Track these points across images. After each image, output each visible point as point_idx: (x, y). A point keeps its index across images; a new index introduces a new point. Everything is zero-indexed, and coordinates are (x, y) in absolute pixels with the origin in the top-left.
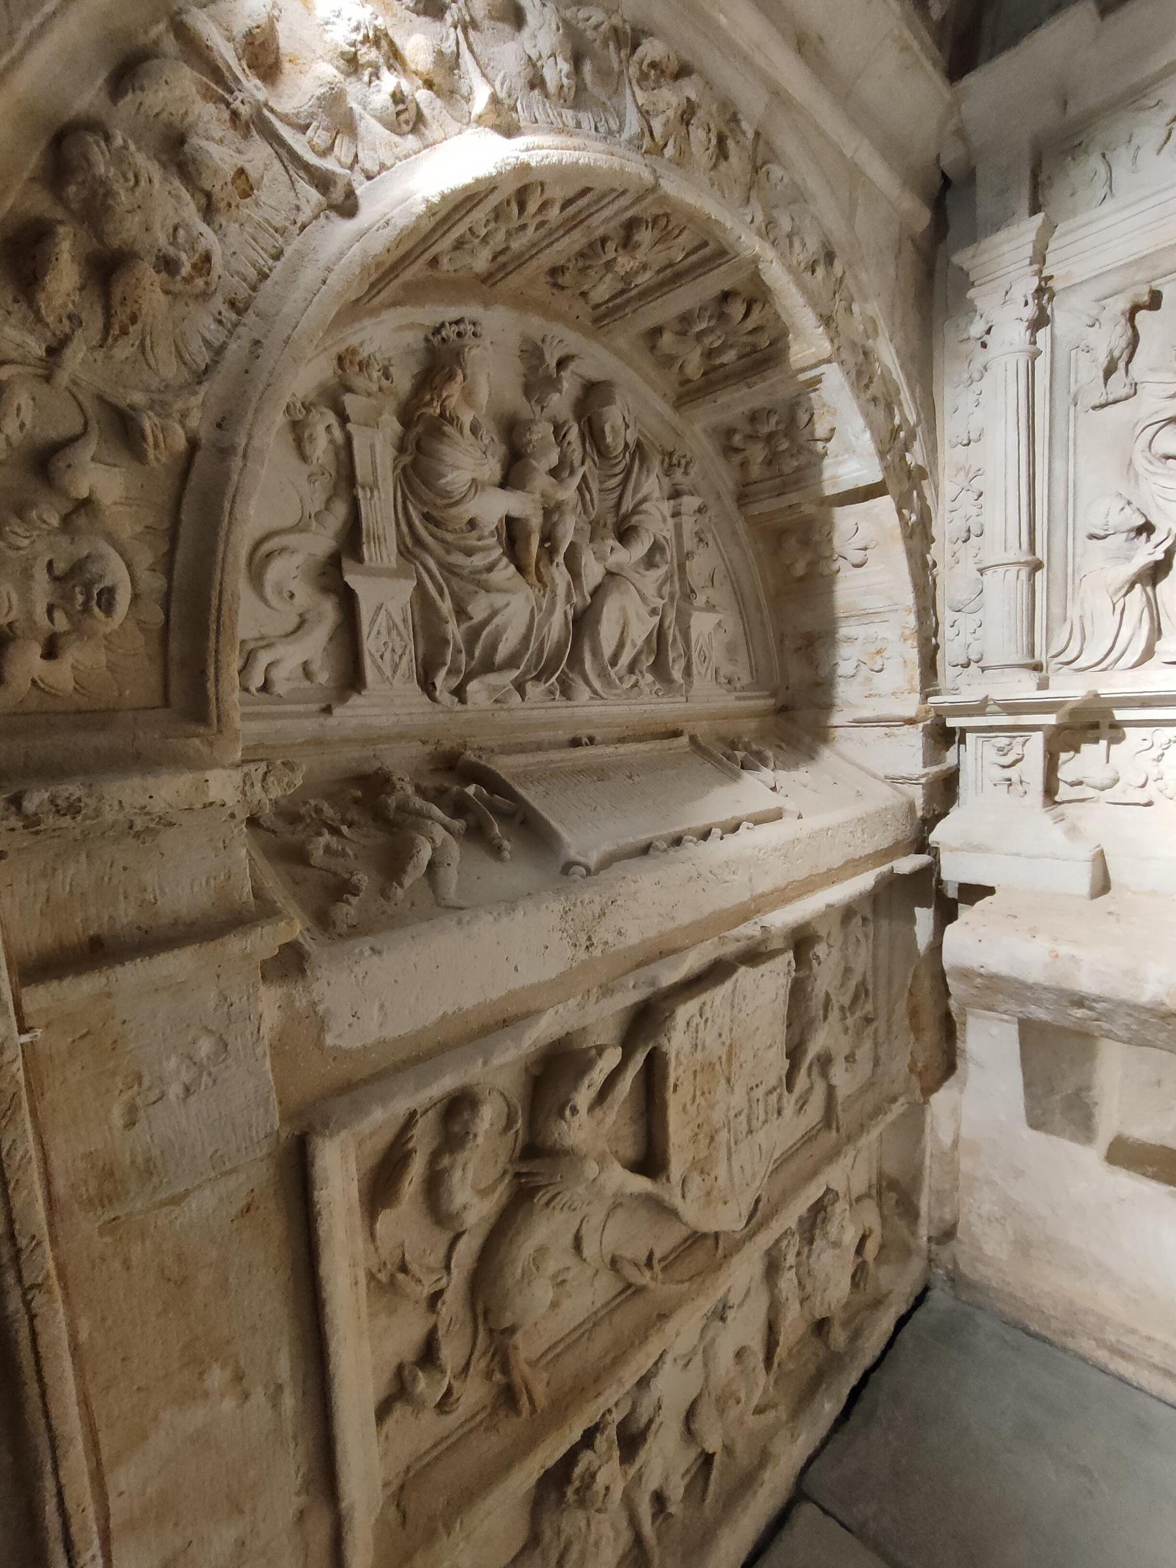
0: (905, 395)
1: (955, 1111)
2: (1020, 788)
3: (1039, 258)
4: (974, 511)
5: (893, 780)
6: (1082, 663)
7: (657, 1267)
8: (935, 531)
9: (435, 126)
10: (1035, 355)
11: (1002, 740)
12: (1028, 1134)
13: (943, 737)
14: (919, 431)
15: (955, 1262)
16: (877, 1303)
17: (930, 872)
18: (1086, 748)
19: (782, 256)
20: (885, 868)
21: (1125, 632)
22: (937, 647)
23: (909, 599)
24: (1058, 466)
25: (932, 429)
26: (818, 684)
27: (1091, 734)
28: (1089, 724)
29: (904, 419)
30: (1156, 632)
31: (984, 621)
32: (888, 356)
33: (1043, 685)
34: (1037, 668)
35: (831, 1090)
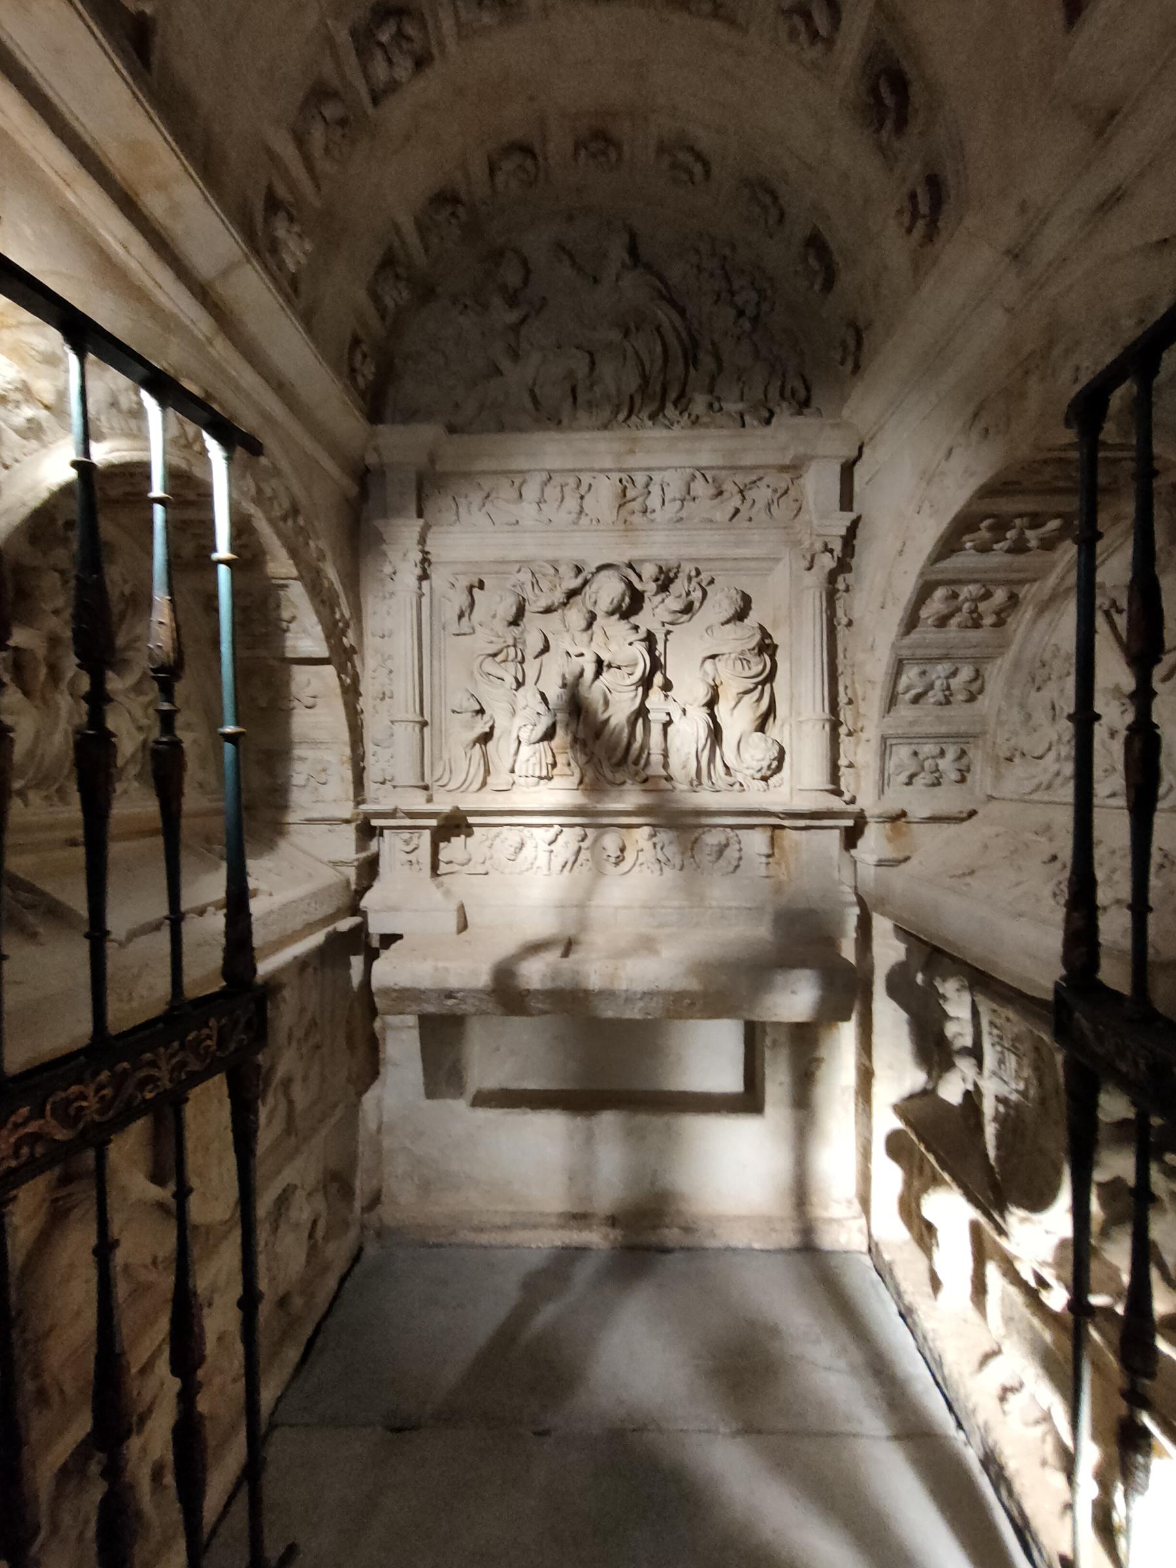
0: (343, 600)
1: (379, 1102)
2: (417, 867)
3: (422, 541)
4: (387, 681)
5: (335, 864)
6: (451, 786)
7: (160, 1267)
8: (362, 689)
9: (49, 433)
10: (421, 596)
11: (406, 835)
12: (429, 1102)
13: (367, 831)
14: (351, 623)
15: (381, 1220)
16: (326, 1269)
17: (360, 930)
18: (453, 839)
19: (265, 512)
20: (330, 928)
21: (472, 771)
22: (364, 768)
23: (345, 735)
24: (435, 663)
25: (359, 620)
26: (276, 791)
27: (456, 831)
28: (453, 825)
29: (343, 615)
30: (487, 772)
31: (392, 756)
32: (331, 574)
33: (430, 800)
34: (426, 788)
35: (291, 1102)
